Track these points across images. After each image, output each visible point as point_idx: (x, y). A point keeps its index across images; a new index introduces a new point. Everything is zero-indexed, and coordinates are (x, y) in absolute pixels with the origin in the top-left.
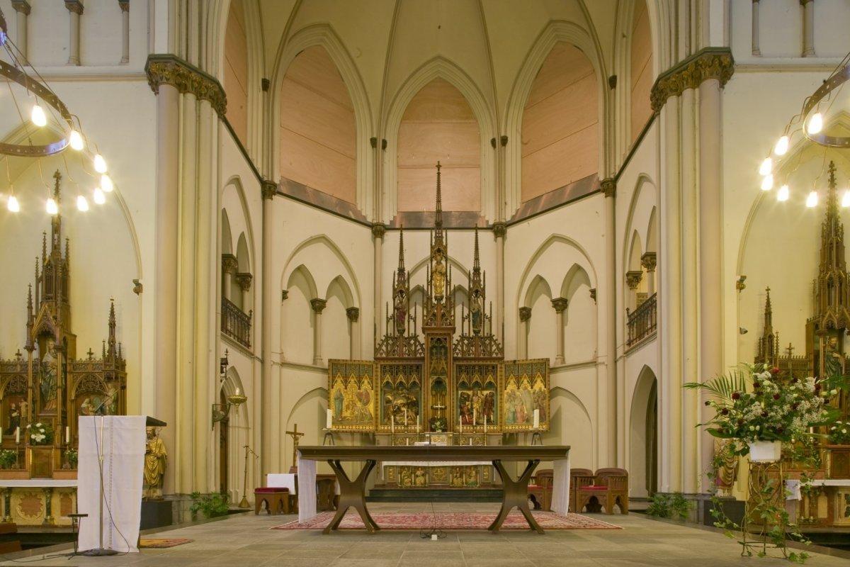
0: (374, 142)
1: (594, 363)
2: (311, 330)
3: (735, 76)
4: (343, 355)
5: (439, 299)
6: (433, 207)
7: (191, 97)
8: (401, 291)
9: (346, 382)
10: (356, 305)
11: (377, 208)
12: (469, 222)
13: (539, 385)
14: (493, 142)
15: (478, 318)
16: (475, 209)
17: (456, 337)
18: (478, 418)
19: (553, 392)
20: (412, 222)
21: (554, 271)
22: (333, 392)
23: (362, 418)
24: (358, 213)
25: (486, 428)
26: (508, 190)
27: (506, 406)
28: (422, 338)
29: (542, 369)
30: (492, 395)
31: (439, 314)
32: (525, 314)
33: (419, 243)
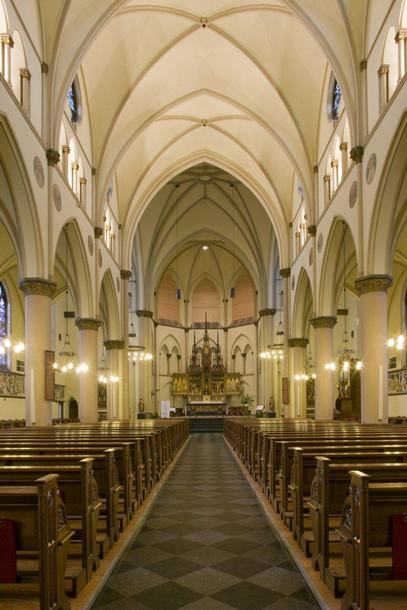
0: (185, 301)
1: (252, 374)
2: (167, 364)
3: (277, 312)
4: (176, 372)
5: (206, 355)
6: (204, 321)
7: (147, 318)
8: (195, 351)
9: (178, 380)
10: (180, 354)
11: (186, 323)
12: (216, 326)
13: (237, 380)
14: (223, 300)
15: (219, 359)
16: (218, 321)
17: (212, 365)
18: (219, 390)
19: (241, 383)
20: (198, 326)
21: (242, 344)
22: (174, 383)
23: (182, 391)
24: (180, 324)
25: (221, 393)
26: (228, 317)
27: (227, 387)
28: (201, 366)
29: (238, 375)
30: (223, 383)
31: (206, 358)
32: (234, 357)
33: (201, 333)
